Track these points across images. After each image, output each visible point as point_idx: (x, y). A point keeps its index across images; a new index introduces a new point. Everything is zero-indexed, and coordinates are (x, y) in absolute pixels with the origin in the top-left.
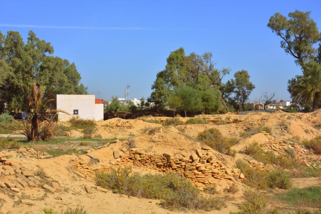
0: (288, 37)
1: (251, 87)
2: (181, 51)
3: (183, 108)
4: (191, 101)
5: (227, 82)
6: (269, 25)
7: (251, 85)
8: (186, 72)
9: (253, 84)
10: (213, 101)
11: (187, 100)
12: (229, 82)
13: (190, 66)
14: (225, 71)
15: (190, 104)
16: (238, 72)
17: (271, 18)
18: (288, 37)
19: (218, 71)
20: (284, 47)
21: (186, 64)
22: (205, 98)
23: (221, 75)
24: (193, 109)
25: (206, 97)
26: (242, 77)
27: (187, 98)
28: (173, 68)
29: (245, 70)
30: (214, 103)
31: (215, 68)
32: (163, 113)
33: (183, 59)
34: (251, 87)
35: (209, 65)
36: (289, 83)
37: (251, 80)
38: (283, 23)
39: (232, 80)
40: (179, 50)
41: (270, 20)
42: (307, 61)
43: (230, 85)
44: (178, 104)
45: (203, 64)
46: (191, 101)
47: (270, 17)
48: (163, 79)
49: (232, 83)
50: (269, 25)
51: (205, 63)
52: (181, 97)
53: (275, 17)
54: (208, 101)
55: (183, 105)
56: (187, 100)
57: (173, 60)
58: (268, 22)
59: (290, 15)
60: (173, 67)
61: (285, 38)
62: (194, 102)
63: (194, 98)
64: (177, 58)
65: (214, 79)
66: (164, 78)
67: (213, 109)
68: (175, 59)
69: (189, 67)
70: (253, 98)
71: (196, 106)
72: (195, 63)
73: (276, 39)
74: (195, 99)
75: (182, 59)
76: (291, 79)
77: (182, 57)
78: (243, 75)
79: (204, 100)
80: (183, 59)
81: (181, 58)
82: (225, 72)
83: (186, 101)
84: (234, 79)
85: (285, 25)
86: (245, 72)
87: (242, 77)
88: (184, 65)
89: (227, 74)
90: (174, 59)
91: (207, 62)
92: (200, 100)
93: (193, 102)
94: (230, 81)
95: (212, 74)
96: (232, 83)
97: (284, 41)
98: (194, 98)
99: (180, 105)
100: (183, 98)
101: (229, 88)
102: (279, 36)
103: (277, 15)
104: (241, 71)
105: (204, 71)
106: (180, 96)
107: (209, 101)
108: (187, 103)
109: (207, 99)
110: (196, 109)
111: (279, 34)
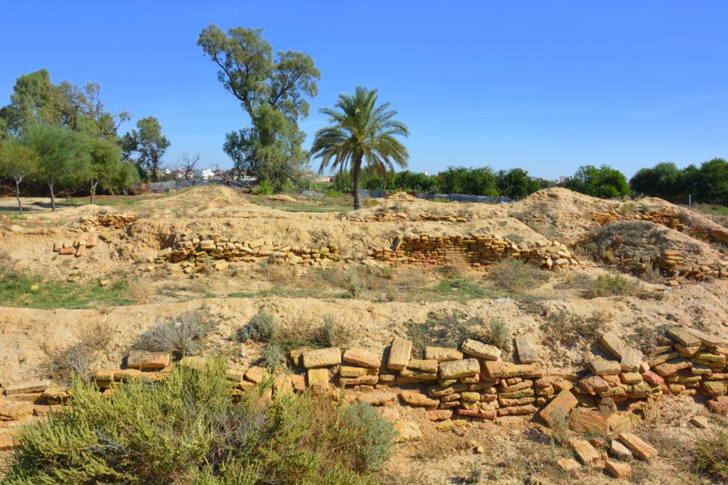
0: (228, 65)
1: (164, 144)
2: (44, 74)
3: (43, 177)
4: (64, 159)
5: (125, 134)
6: (200, 42)
7: (164, 140)
8: (54, 111)
9: (167, 138)
10: (116, 162)
11: (54, 156)
12: (128, 134)
13: (61, 102)
14: (124, 115)
15: (61, 166)
16: (142, 119)
17: (203, 32)
18: (228, 65)
19: (110, 116)
20: (223, 81)
21: (52, 98)
22: (98, 155)
23: (117, 121)
24: (70, 180)
25: (100, 153)
26: (149, 130)
27: (54, 151)
28: (26, 100)
29: (154, 116)
30: (118, 167)
31: (105, 110)
32: (11, 184)
33: (47, 88)
34: (164, 144)
35: (95, 103)
36: (228, 138)
37: (164, 133)
38: (223, 41)
39: (134, 132)
40: (38, 72)
41: (201, 36)
42: (255, 106)
43: (130, 139)
44: (29, 167)
45: (84, 101)
46: (64, 159)
47: (201, 30)
48: (5, 121)
49: (133, 136)
50: (200, 42)
51: (88, 101)
52: (38, 149)
53: (208, 30)
54: (104, 162)
55: (43, 170)
56: (54, 156)
57: (26, 87)
58: (198, 37)
59: (231, 32)
60: (25, 99)
61: (225, 67)
62: (72, 162)
63: (72, 153)
64: (35, 83)
65: (105, 126)
66: (8, 119)
67: (117, 179)
68: (30, 85)
69: (59, 103)
70: (170, 161)
71: (79, 171)
72: (70, 98)
73: (210, 69)
74: (77, 155)
75: (45, 88)
76: (230, 133)
77: (45, 84)
78: (151, 124)
79: (96, 159)
80: (47, 88)
81: (43, 87)
82: (124, 116)
83: (51, 160)
84: (137, 130)
85: (226, 43)
86: (154, 120)
87: (149, 130)
88: (48, 98)
89: (127, 120)
90: (27, 84)
91: (93, 98)
92: (87, 158)
93: (70, 162)
94: (131, 133)
95: (102, 119)
96: (133, 136)
97: (223, 71)
98: (72, 153)
99: (33, 169)
100: (44, 150)
101: (130, 145)
102: (216, 63)
103: (211, 27)
104: (147, 117)
105: (87, 113)
106: (34, 146)
107: (107, 163)
108: (55, 164)
109: (103, 156)
110: (77, 180)
111: (215, 59)
